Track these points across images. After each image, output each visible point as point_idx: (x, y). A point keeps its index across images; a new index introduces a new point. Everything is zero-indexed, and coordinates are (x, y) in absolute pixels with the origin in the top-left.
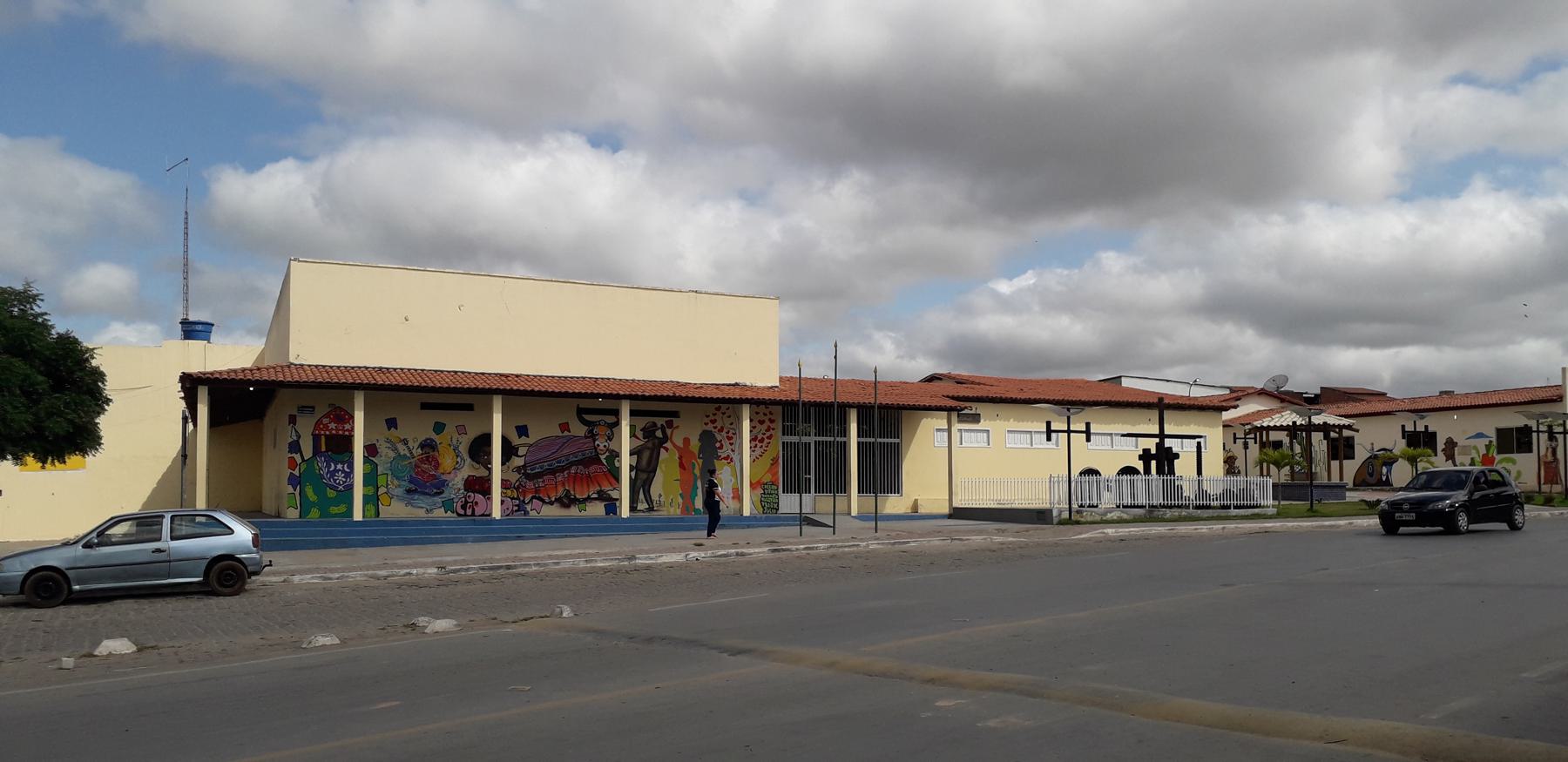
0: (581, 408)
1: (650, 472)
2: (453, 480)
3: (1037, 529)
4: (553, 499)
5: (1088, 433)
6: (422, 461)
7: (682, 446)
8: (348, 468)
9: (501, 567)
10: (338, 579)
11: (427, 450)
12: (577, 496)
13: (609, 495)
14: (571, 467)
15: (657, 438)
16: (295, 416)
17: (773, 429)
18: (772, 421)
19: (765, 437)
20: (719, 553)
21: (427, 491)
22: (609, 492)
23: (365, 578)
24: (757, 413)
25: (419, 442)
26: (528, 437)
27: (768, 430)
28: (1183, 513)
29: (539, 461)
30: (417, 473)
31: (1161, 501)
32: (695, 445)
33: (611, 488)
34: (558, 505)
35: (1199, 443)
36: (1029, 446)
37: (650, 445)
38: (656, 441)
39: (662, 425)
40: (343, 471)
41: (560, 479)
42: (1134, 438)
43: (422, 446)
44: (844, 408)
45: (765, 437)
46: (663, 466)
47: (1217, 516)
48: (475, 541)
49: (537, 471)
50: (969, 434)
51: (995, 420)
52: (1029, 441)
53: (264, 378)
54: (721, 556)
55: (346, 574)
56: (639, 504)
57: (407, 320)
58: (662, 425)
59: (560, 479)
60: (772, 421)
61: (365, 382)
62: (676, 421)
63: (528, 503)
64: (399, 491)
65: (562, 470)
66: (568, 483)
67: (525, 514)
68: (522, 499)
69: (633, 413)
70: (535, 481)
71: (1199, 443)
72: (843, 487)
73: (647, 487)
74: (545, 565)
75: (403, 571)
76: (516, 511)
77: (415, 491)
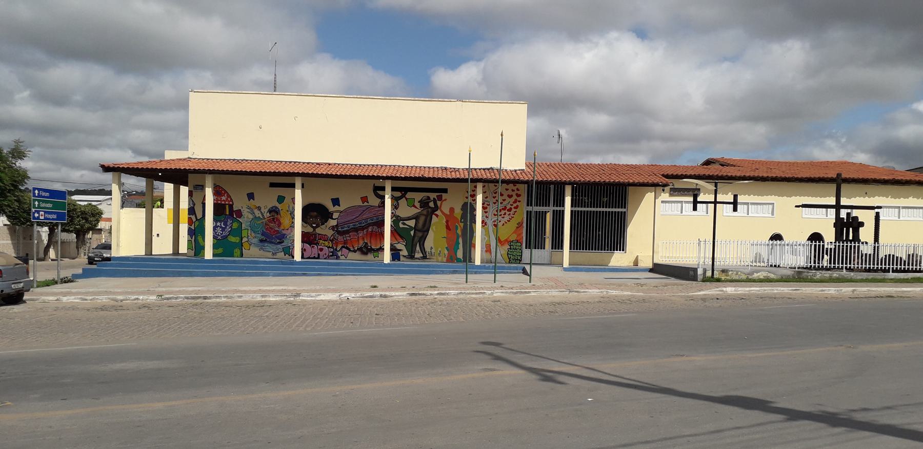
0: (376, 186)
1: (425, 231)
2: (290, 234)
3: (676, 284)
4: (356, 249)
5: (735, 204)
6: (270, 221)
7: (448, 213)
8: (224, 225)
9: (200, 297)
10: (91, 300)
11: (273, 214)
12: (373, 247)
13: (395, 247)
14: (369, 227)
15: (430, 207)
16: (192, 191)
17: (520, 201)
18: (518, 195)
19: (512, 207)
20: (367, 295)
21: (273, 241)
22: (395, 245)
23: (108, 300)
24: (507, 190)
25: (268, 208)
26: (339, 206)
27: (515, 201)
28: (835, 275)
29: (345, 223)
30: (267, 229)
31: (813, 264)
32: (458, 212)
33: (397, 242)
34: (360, 252)
35: (878, 214)
36: (897, 219)
37: (425, 212)
38: (429, 209)
39: (434, 199)
40: (221, 227)
41: (361, 235)
42: (824, 209)
43: (270, 211)
44: (560, 186)
45: (512, 207)
46: (434, 227)
47: (872, 279)
48: (275, 275)
49: (345, 229)
50: (907, 210)
51: (864, 197)
52: (705, 210)
53: (448, 177)
54: (366, 297)
55: (97, 297)
56: (416, 254)
57: (261, 128)
58: (434, 199)
59: (361, 235)
60: (518, 195)
61: (521, 179)
62: (444, 196)
63: (339, 251)
64: (255, 241)
65: (363, 229)
66: (367, 238)
67: (337, 259)
68: (335, 248)
69: (393, 189)
70: (344, 236)
71: (878, 214)
72: (543, 247)
73: (422, 243)
74: (231, 297)
75: (133, 297)
76: (331, 256)
77: (265, 241)
